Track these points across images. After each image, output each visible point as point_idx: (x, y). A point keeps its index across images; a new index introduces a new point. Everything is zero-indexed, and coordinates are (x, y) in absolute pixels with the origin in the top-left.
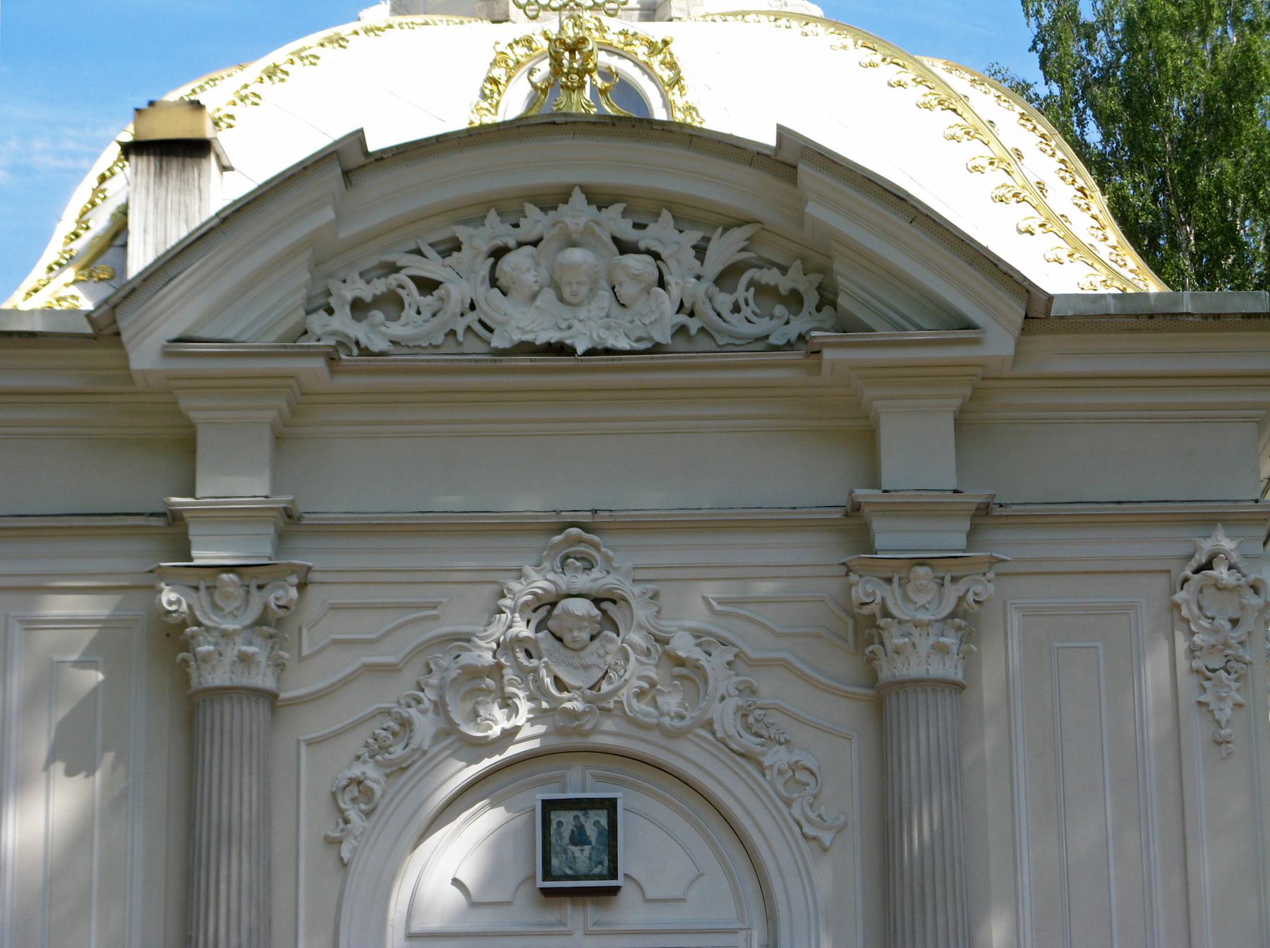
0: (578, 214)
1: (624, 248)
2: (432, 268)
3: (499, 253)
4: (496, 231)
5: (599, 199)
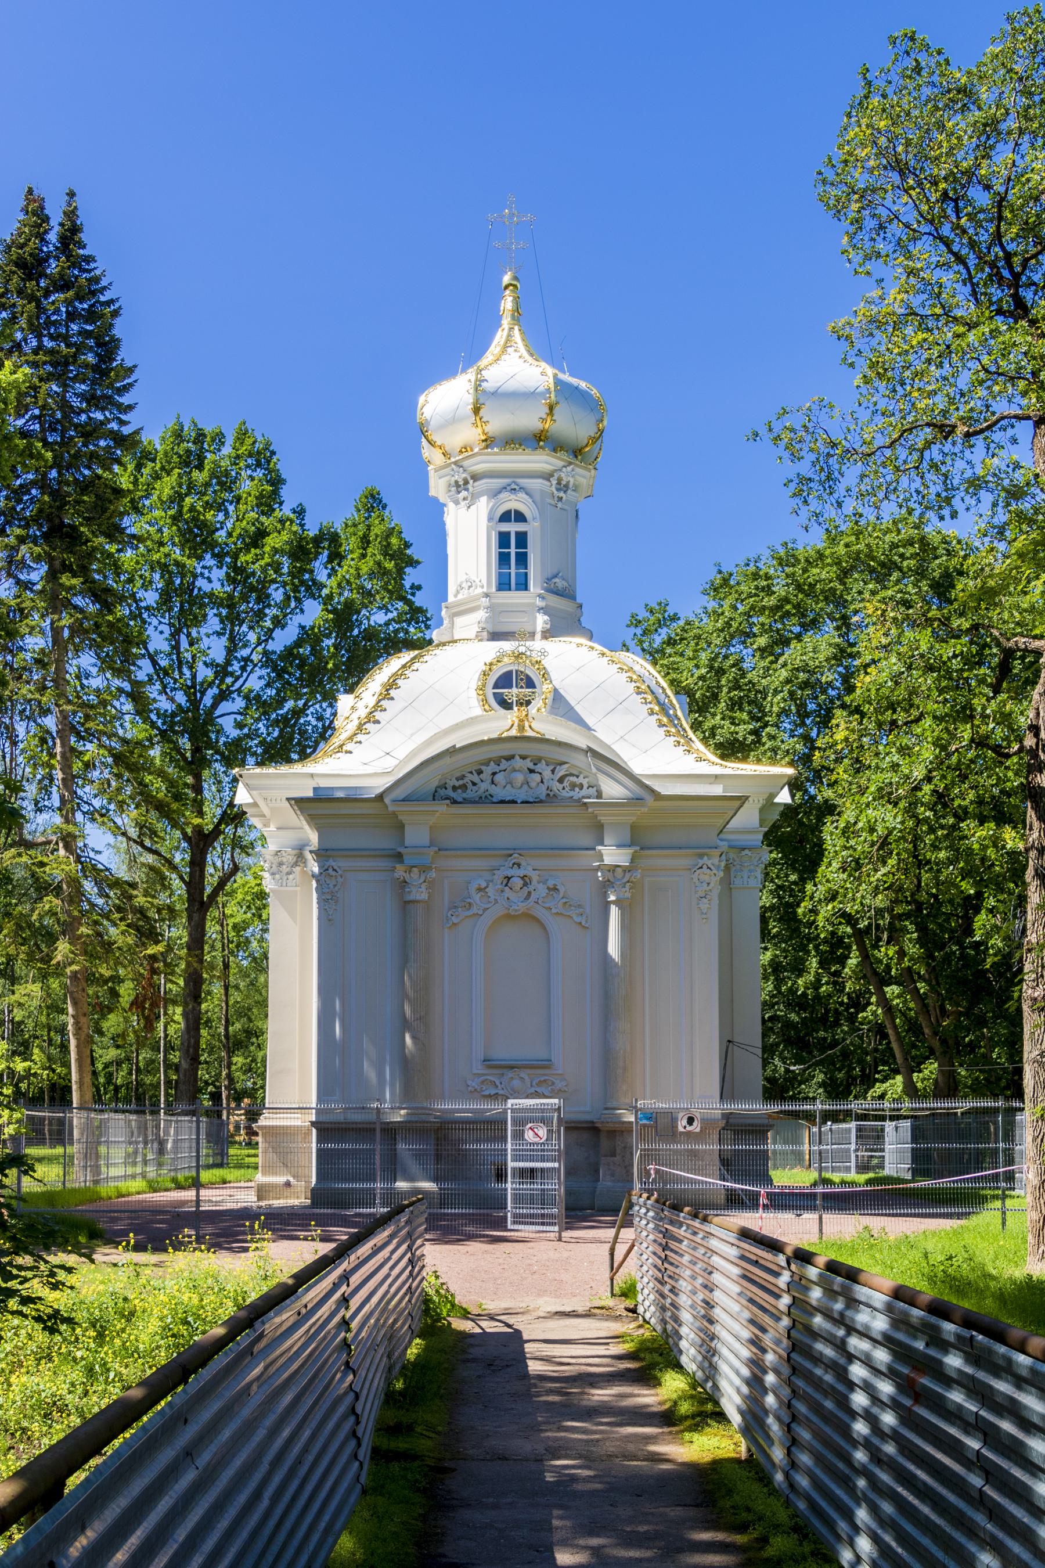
0: (518, 763)
1: (531, 771)
2: (475, 778)
3: (494, 774)
4: (493, 767)
5: (523, 757)
